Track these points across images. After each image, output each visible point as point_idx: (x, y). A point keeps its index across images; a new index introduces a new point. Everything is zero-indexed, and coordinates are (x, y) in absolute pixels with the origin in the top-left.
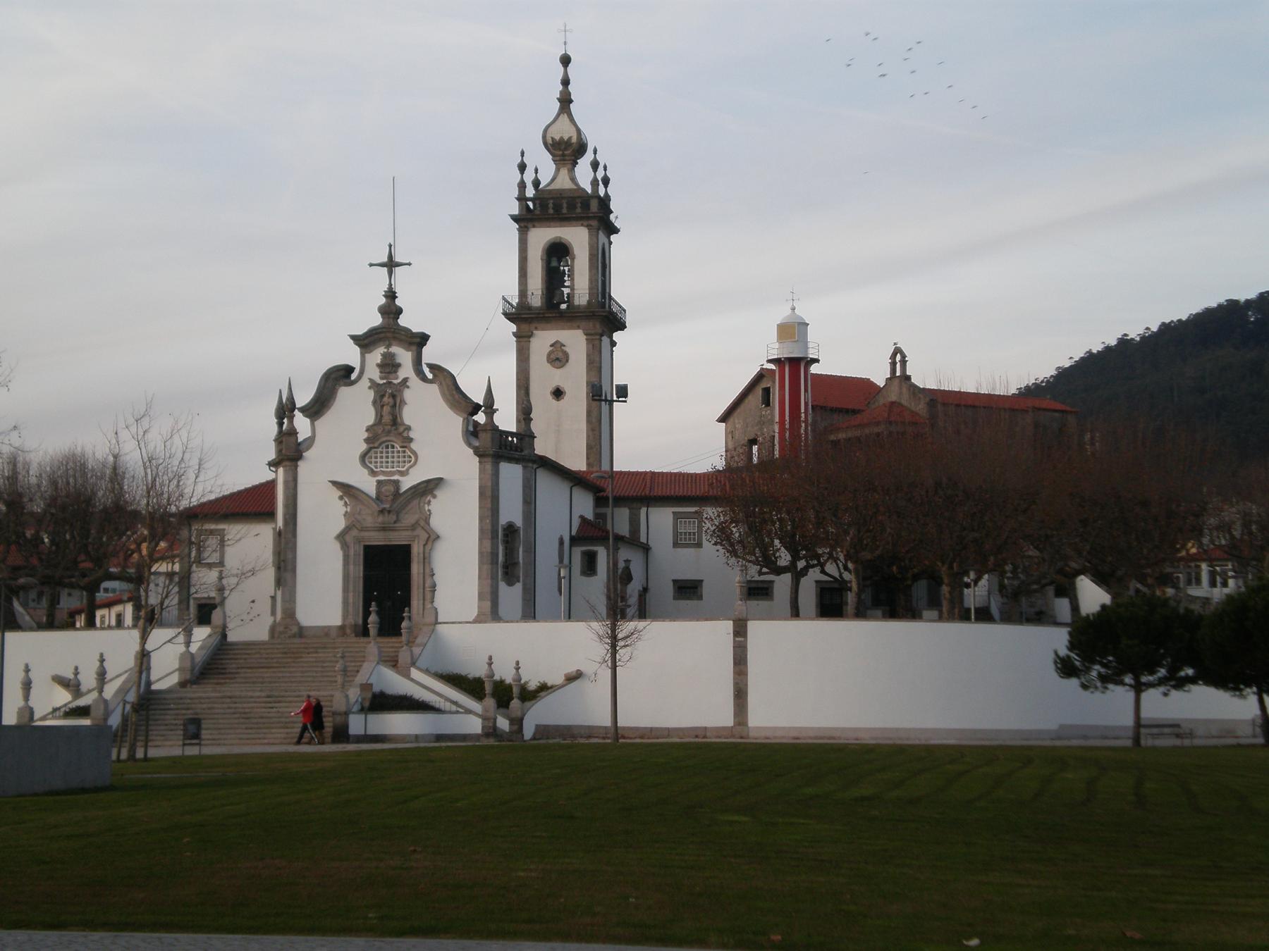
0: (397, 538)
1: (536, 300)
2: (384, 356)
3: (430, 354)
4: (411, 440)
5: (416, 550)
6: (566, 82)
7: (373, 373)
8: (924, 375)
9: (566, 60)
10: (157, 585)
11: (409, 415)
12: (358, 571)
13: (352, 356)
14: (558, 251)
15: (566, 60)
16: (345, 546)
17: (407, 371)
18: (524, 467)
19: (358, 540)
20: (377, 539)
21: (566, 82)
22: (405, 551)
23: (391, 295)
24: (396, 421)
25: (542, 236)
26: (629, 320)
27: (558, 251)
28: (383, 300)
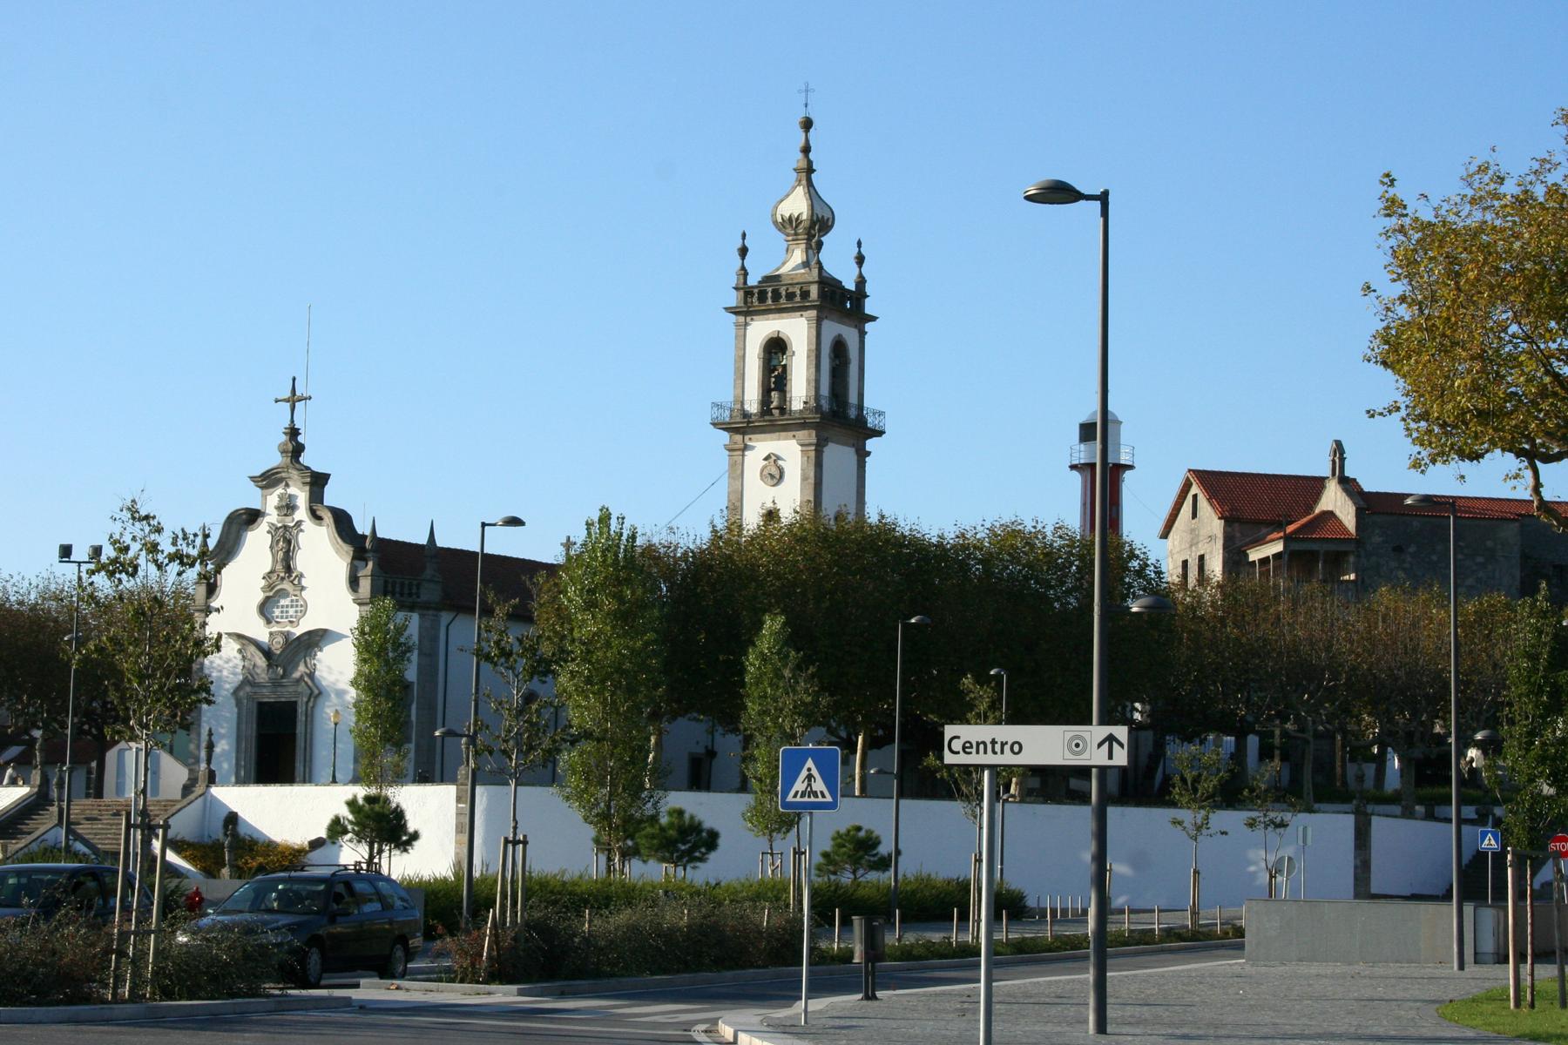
0: (285, 695)
1: (752, 406)
2: (281, 497)
3: (332, 496)
4: (303, 588)
5: (301, 709)
6: (806, 150)
7: (272, 517)
8: (441, 542)
9: (807, 124)
10: (1512, 722)
11: (301, 562)
12: (251, 730)
13: (251, 498)
14: (776, 347)
15: (807, 124)
16: (239, 703)
17: (302, 513)
18: (422, 616)
19: (298, 694)
20: (268, 696)
21: (806, 150)
22: (292, 706)
23: (293, 432)
24: (288, 569)
25: (761, 329)
26: (889, 425)
27: (776, 347)
28: (284, 438)
